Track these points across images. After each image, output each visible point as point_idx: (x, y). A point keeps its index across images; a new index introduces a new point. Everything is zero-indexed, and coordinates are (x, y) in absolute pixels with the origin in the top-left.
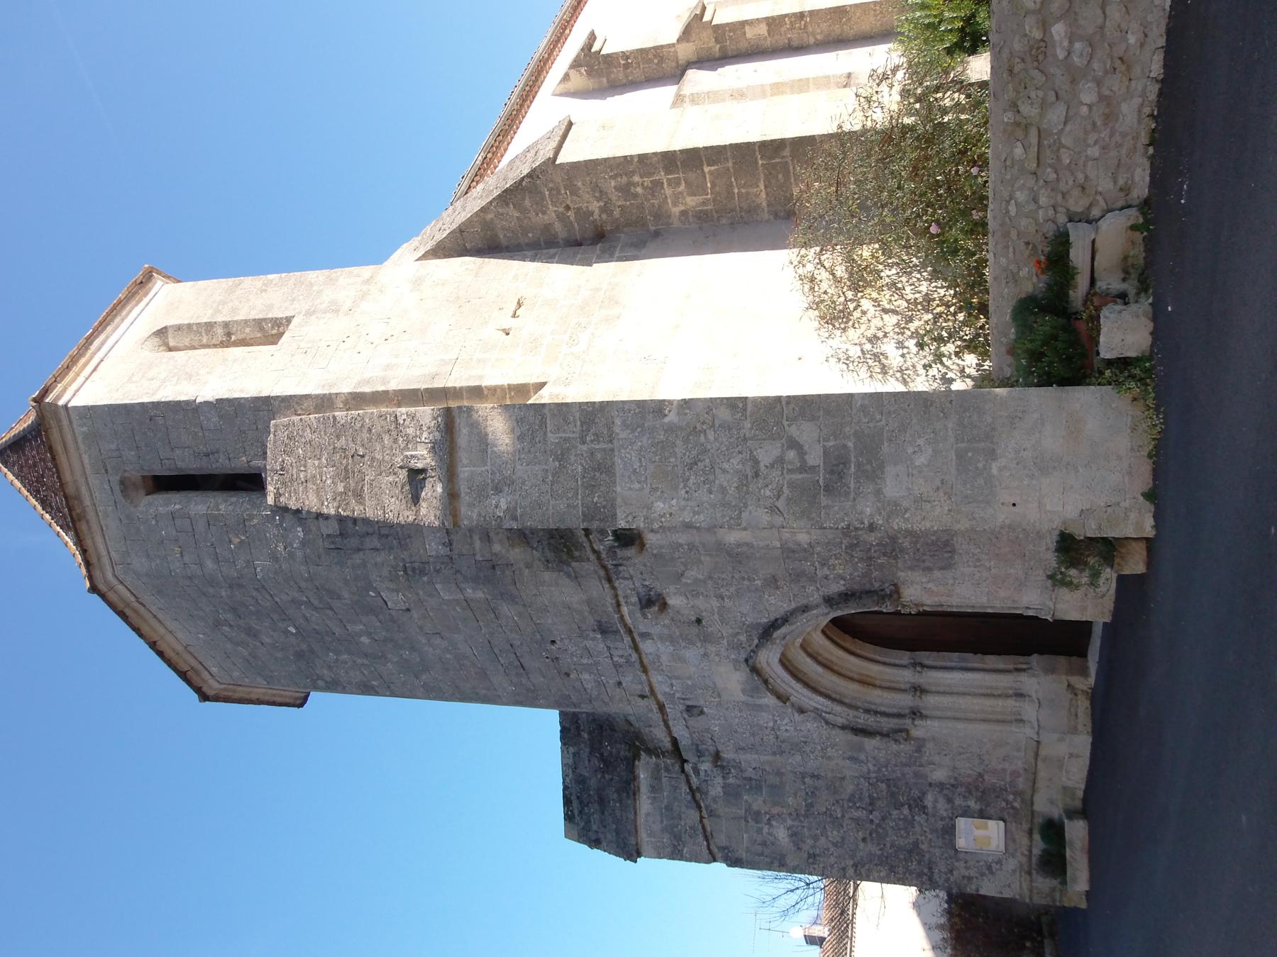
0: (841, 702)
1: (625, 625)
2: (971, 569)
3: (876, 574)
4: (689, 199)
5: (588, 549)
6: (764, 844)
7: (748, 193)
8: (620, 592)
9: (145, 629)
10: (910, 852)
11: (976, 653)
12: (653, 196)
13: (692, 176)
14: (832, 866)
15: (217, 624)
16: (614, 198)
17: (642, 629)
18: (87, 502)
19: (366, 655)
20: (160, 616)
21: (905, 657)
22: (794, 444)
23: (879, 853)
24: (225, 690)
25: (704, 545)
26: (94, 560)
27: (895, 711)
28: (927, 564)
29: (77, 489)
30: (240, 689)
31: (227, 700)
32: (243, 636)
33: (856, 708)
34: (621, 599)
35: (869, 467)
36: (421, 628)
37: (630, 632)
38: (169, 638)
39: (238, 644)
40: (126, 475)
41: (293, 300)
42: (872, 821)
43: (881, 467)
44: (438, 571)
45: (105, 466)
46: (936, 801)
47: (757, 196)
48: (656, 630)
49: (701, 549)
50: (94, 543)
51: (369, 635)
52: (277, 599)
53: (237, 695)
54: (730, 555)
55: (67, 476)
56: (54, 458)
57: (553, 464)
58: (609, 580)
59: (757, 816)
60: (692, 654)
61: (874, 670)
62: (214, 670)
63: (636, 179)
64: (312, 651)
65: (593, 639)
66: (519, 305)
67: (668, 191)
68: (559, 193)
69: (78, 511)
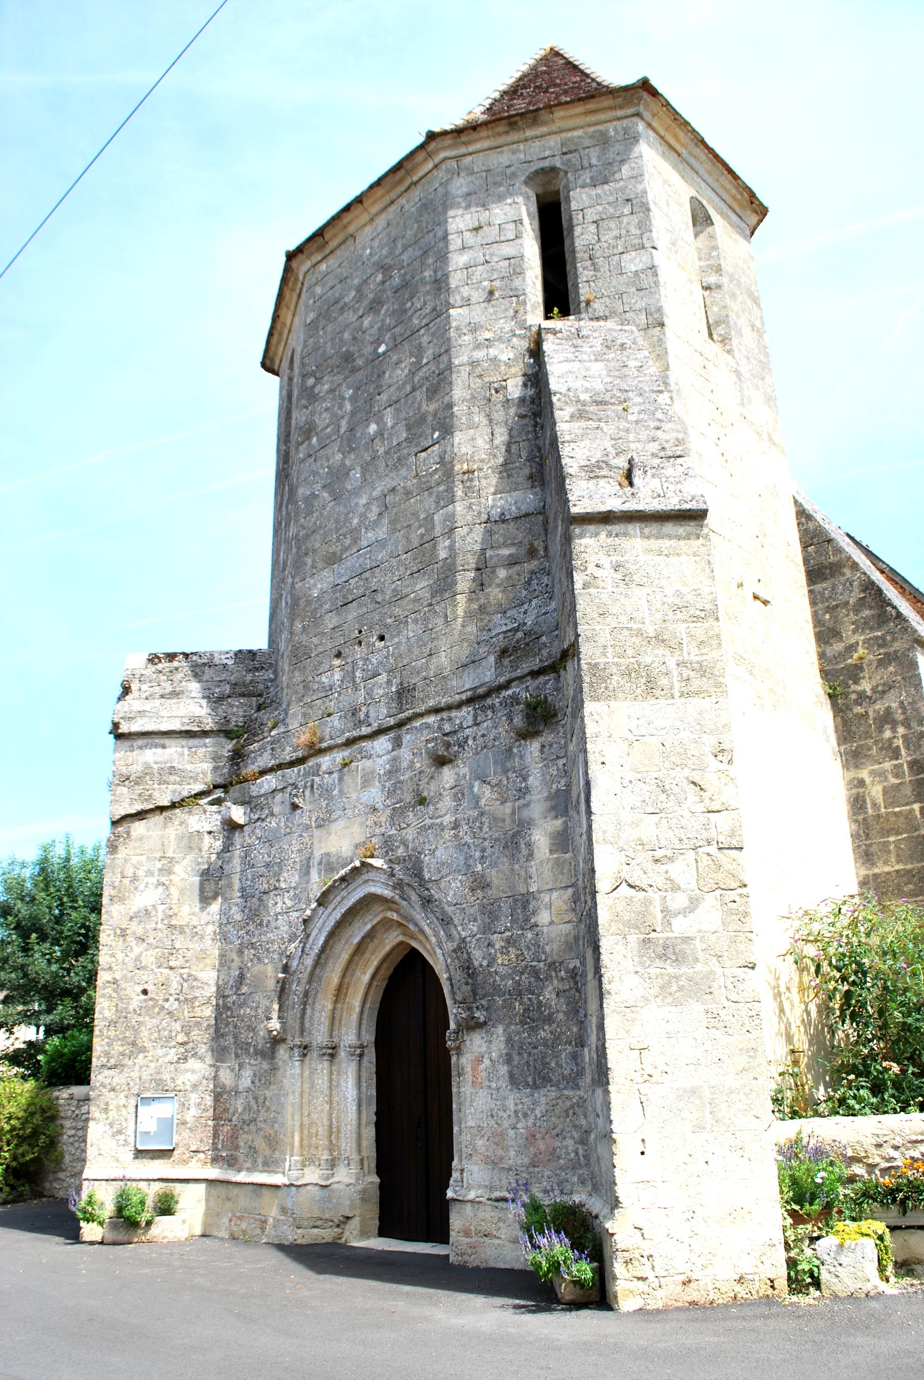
0: (317, 964)
1: (410, 719)
2: (512, 1107)
3: (499, 1001)
4: (879, 788)
5: (514, 675)
6: (135, 878)
7: (889, 852)
8: (454, 714)
9: (379, 192)
10: (134, 1044)
11: (377, 1114)
12: (882, 749)
13: (908, 791)
14: (113, 955)
15: (386, 269)
16: (877, 707)
17: (407, 738)
18: (529, 133)
19: (351, 430)
20: (392, 208)
21: (369, 1037)
22: (694, 903)
23: (131, 1008)
24: (296, 279)
25: (527, 805)
26: (464, 138)
27: (307, 1025)
28: (516, 1058)
29: (544, 123)
30: (295, 297)
31: (284, 281)
32: (371, 296)
33: (310, 982)
34: (445, 715)
35: (674, 988)
36: (393, 490)
37: (400, 725)
38: (365, 218)
39: (359, 290)
40: (562, 174)
41: (748, 358)
42: (167, 1000)
43: (677, 1003)
44: (470, 507)
45: (571, 152)
46: (193, 1072)
47: (886, 862)
48: (405, 753)
49: (521, 802)
50: (481, 139)
51: (380, 433)
52: (422, 332)
53: (287, 294)
54: (514, 836)
55: (560, 113)
56: (580, 99)
57: (651, 631)
58: (470, 701)
59: (167, 871)
60: (375, 794)
61: (355, 1000)
62: (323, 267)
63: (901, 730)
64: (354, 370)
65: (389, 682)
66: (765, 603)
67: (888, 765)
68: (880, 646)
69: (520, 123)
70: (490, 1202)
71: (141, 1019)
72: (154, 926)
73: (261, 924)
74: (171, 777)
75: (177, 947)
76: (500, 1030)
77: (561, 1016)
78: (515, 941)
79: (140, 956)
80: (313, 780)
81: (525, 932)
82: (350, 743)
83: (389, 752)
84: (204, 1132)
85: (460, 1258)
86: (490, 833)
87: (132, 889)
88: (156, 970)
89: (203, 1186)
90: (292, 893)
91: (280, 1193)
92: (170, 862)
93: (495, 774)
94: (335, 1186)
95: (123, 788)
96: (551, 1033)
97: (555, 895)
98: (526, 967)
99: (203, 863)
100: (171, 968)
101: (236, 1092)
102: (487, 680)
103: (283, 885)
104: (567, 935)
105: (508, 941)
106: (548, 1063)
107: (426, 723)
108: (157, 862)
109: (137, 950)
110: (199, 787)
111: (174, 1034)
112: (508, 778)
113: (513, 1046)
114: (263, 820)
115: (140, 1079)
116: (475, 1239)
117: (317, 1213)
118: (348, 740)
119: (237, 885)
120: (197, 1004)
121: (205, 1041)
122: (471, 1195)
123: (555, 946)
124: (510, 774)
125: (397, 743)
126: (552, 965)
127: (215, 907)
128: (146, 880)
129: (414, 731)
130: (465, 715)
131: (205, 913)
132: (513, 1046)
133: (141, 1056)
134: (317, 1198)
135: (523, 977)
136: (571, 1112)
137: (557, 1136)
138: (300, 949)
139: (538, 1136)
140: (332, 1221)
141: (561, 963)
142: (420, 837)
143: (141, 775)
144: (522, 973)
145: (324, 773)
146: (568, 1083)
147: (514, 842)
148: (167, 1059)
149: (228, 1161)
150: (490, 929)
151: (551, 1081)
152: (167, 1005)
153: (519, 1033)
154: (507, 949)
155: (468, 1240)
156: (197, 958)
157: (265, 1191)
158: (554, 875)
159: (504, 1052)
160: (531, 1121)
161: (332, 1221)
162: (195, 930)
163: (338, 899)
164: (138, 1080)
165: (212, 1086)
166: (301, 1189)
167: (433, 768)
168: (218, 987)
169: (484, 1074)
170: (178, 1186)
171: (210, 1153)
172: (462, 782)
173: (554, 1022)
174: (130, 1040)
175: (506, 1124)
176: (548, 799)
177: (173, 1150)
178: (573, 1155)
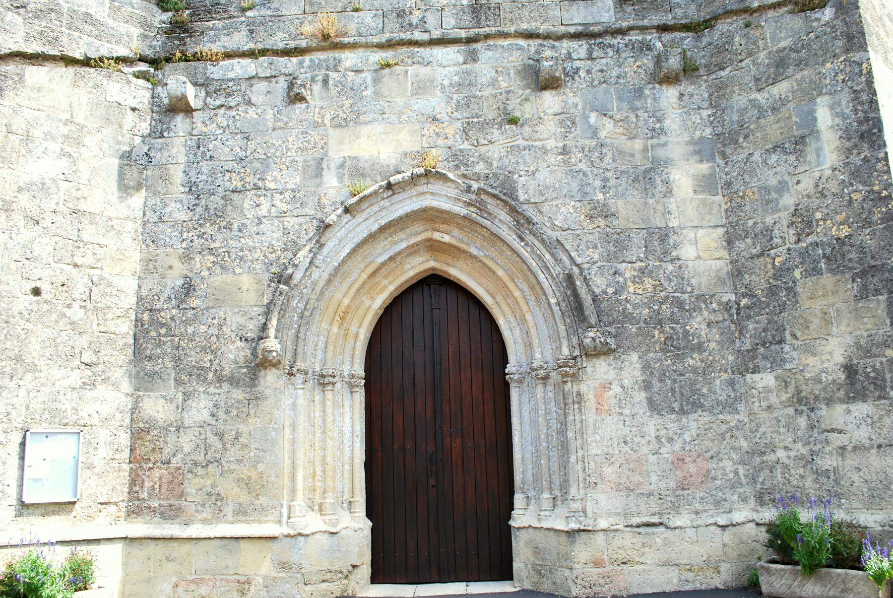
2: (653, 433)
5: (640, 23)
10: (18, 359)
25: (665, 145)
28: (657, 385)
49: (655, 141)
54: (646, 172)
70: (629, 529)
71: (30, 326)
72: (54, 206)
73: (229, 227)
74: (86, 26)
75: (85, 240)
76: (634, 357)
77: (713, 345)
78: (651, 272)
79: (31, 242)
80: (327, 75)
81: (664, 265)
82: (390, 45)
83: (458, 64)
84: (116, 478)
85: (588, 590)
86: (614, 165)
87: (23, 151)
88: (53, 265)
89: (119, 547)
90: (287, 195)
91: (275, 545)
92: (79, 130)
93: (619, 109)
94: (343, 533)
95: (16, 16)
96: (702, 361)
97: (701, 233)
98: (668, 297)
99: (124, 144)
100: (76, 266)
101: (178, 429)
102: (603, 20)
103: (272, 185)
104: (718, 271)
105: (642, 271)
106: (699, 390)
107: (517, 45)
108: (61, 125)
109: (27, 234)
110: (122, 52)
111: (77, 351)
112: (637, 116)
113: (651, 373)
114: (230, 108)
115: (27, 408)
116: (609, 568)
117: (326, 566)
118: (388, 41)
119: (178, 176)
120: (110, 316)
121: (120, 363)
122: (603, 524)
123: (704, 280)
124: (640, 113)
125: (473, 57)
126: (701, 297)
127: (138, 200)
128: (45, 144)
129: (500, 50)
130: (580, 48)
131: (124, 204)
132: (651, 373)
133: (29, 376)
134: (326, 548)
135: (664, 307)
136: (728, 435)
137: (712, 458)
138: (308, 260)
139: (687, 460)
140: (341, 572)
141: (713, 296)
142: (510, 156)
143: (44, 8)
144: (662, 303)
145: (347, 70)
146: (724, 408)
147: (649, 176)
148: (66, 383)
149: (162, 513)
150: (617, 258)
151: (702, 406)
152: (69, 313)
153: (660, 360)
154: (640, 278)
155: (600, 570)
156: (113, 258)
157: (243, 545)
158: (700, 214)
159: (640, 379)
160: (678, 446)
161: (341, 572)
162: (111, 223)
163: (375, 208)
164: (23, 409)
165: (128, 421)
166: (308, 538)
167: (528, 91)
168: (140, 299)
169: (613, 401)
170: (92, 548)
171: (125, 504)
172: (572, 111)
173: (705, 351)
174: (12, 354)
175: (645, 450)
176: (689, 143)
177: (75, 502)
178: (731, 476)
